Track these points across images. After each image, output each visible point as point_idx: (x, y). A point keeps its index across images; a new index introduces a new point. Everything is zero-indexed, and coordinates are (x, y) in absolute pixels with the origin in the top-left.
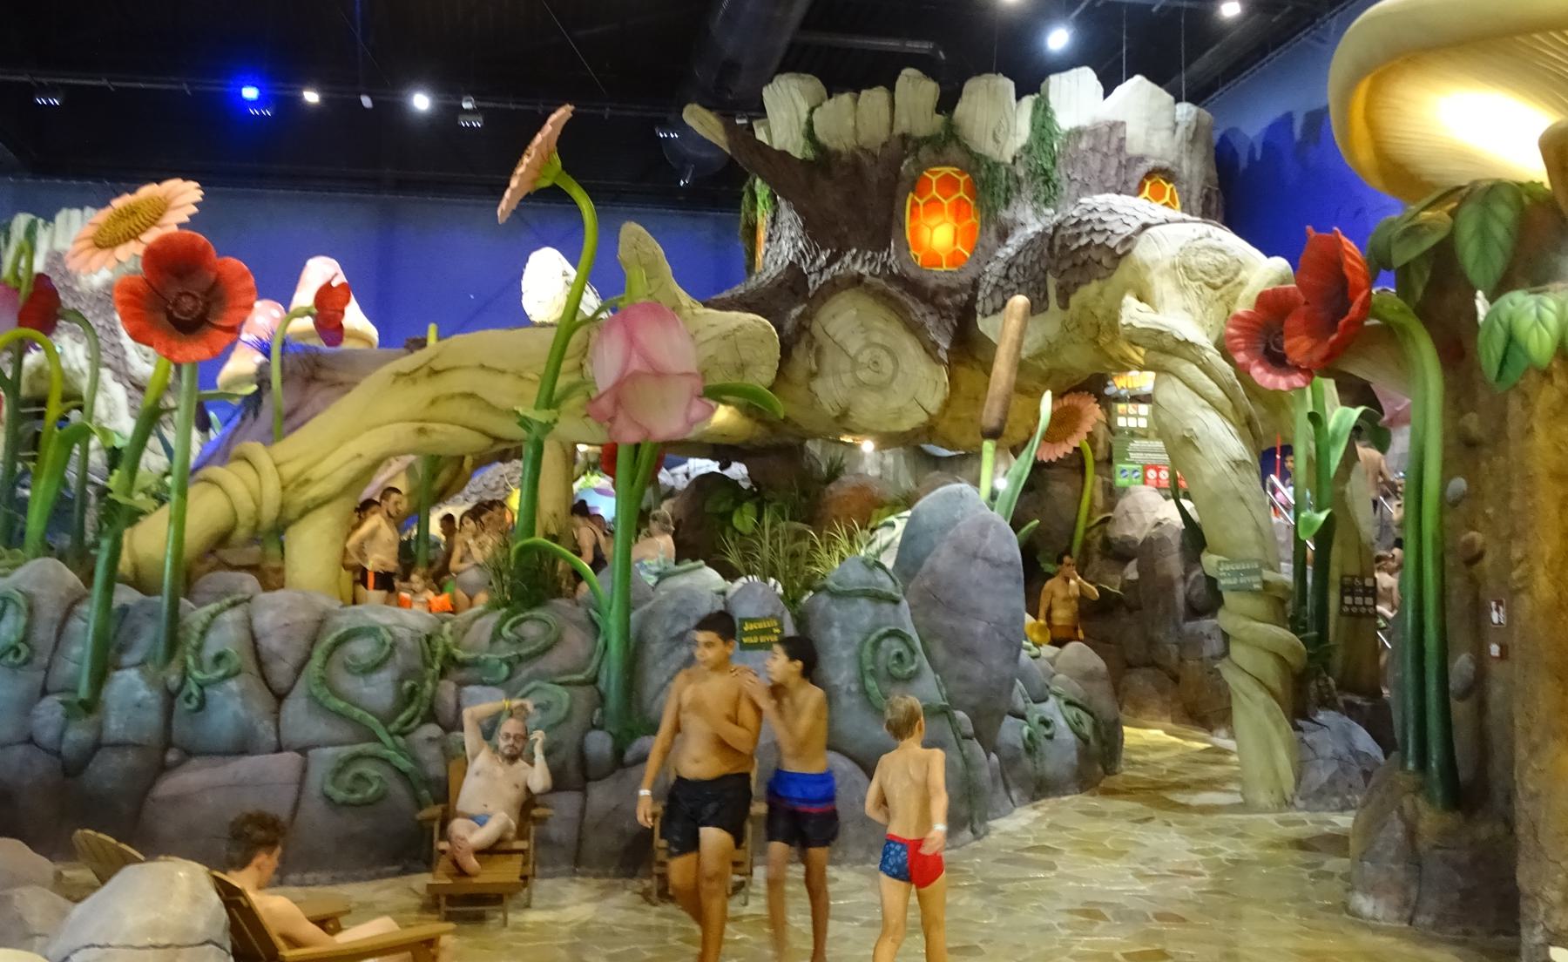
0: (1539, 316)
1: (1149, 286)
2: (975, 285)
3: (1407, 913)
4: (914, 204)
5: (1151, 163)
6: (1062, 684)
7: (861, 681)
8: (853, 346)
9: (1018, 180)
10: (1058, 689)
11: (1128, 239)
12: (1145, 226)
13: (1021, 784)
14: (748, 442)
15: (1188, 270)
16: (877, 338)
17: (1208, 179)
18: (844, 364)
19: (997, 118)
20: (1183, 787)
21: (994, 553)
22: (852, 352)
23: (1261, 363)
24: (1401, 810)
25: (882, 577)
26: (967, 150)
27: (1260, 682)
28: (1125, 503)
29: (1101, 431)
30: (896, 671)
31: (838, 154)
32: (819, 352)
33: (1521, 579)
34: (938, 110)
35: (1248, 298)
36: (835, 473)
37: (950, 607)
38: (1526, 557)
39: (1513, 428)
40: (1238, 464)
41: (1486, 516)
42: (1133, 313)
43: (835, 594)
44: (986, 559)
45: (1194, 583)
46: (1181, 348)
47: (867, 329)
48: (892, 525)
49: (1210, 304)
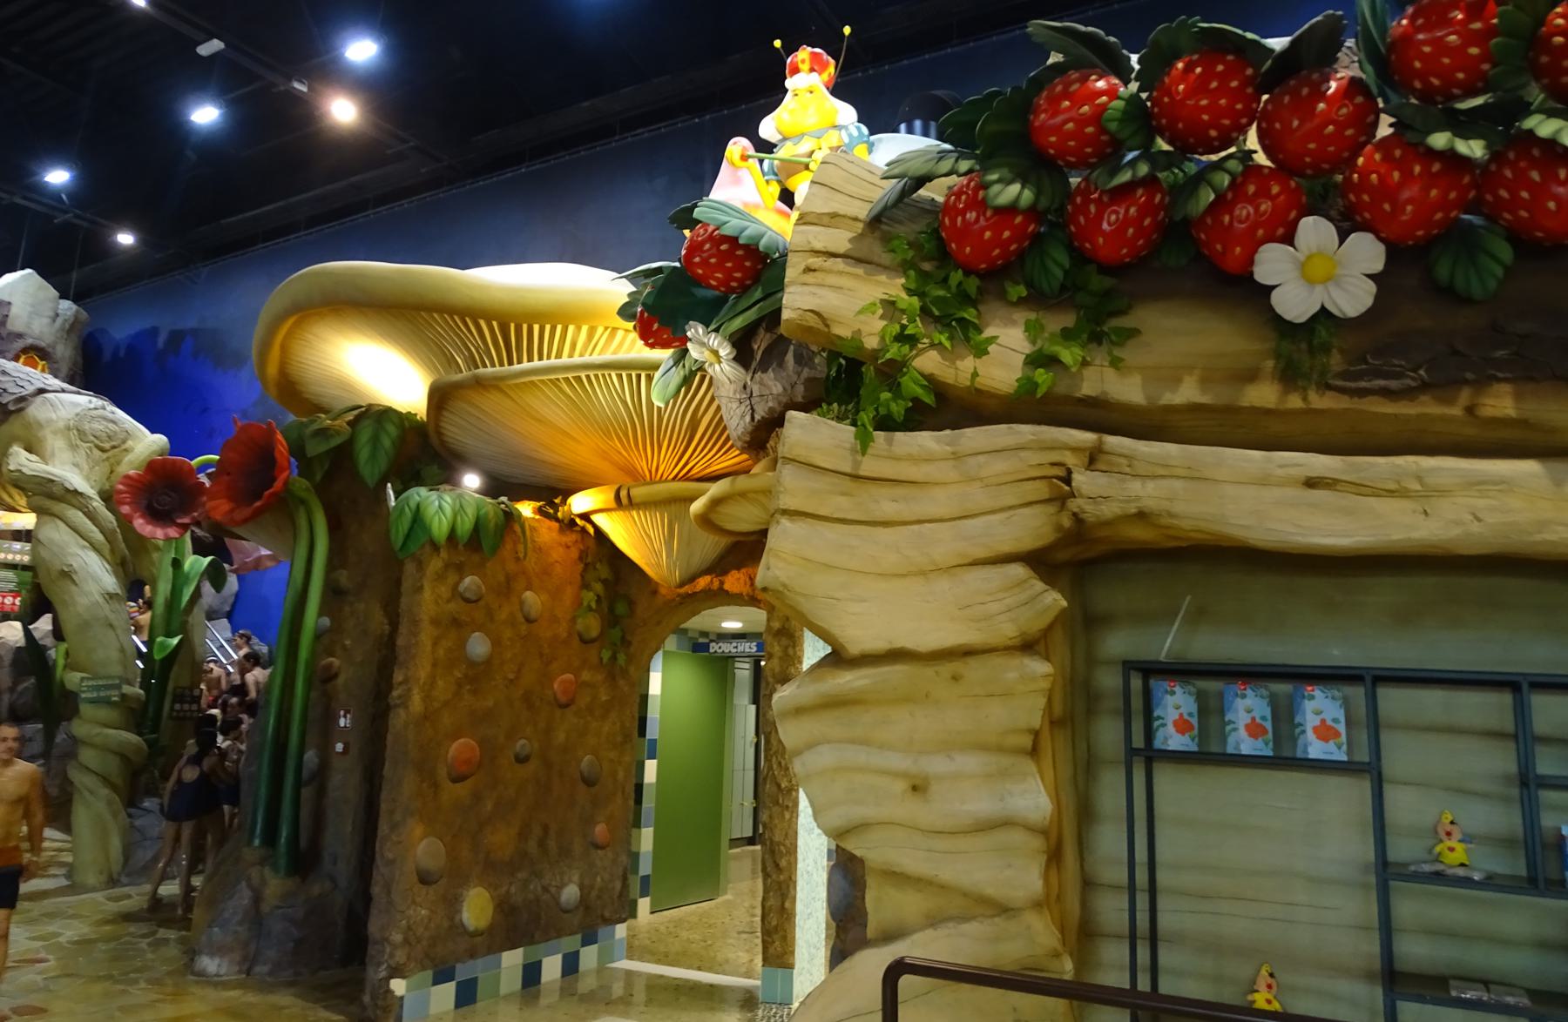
0: (440, 507)
1: (40, 441)
3: (245, 968)
5: (30, 341)
11: (22, 399)
12: (42, 391)
15: (81, 433)
17: (75, 364)
23: (142, 516)
24: (249, 880)
33: (400, 697)
35: (131, 462)
38: (406, 681)
39: (407, 585)
40: (111, 596)
41: (344, 648)
42: (21, 460)
45: (21, 693)
46: (69, 496)
49: (97, 463)
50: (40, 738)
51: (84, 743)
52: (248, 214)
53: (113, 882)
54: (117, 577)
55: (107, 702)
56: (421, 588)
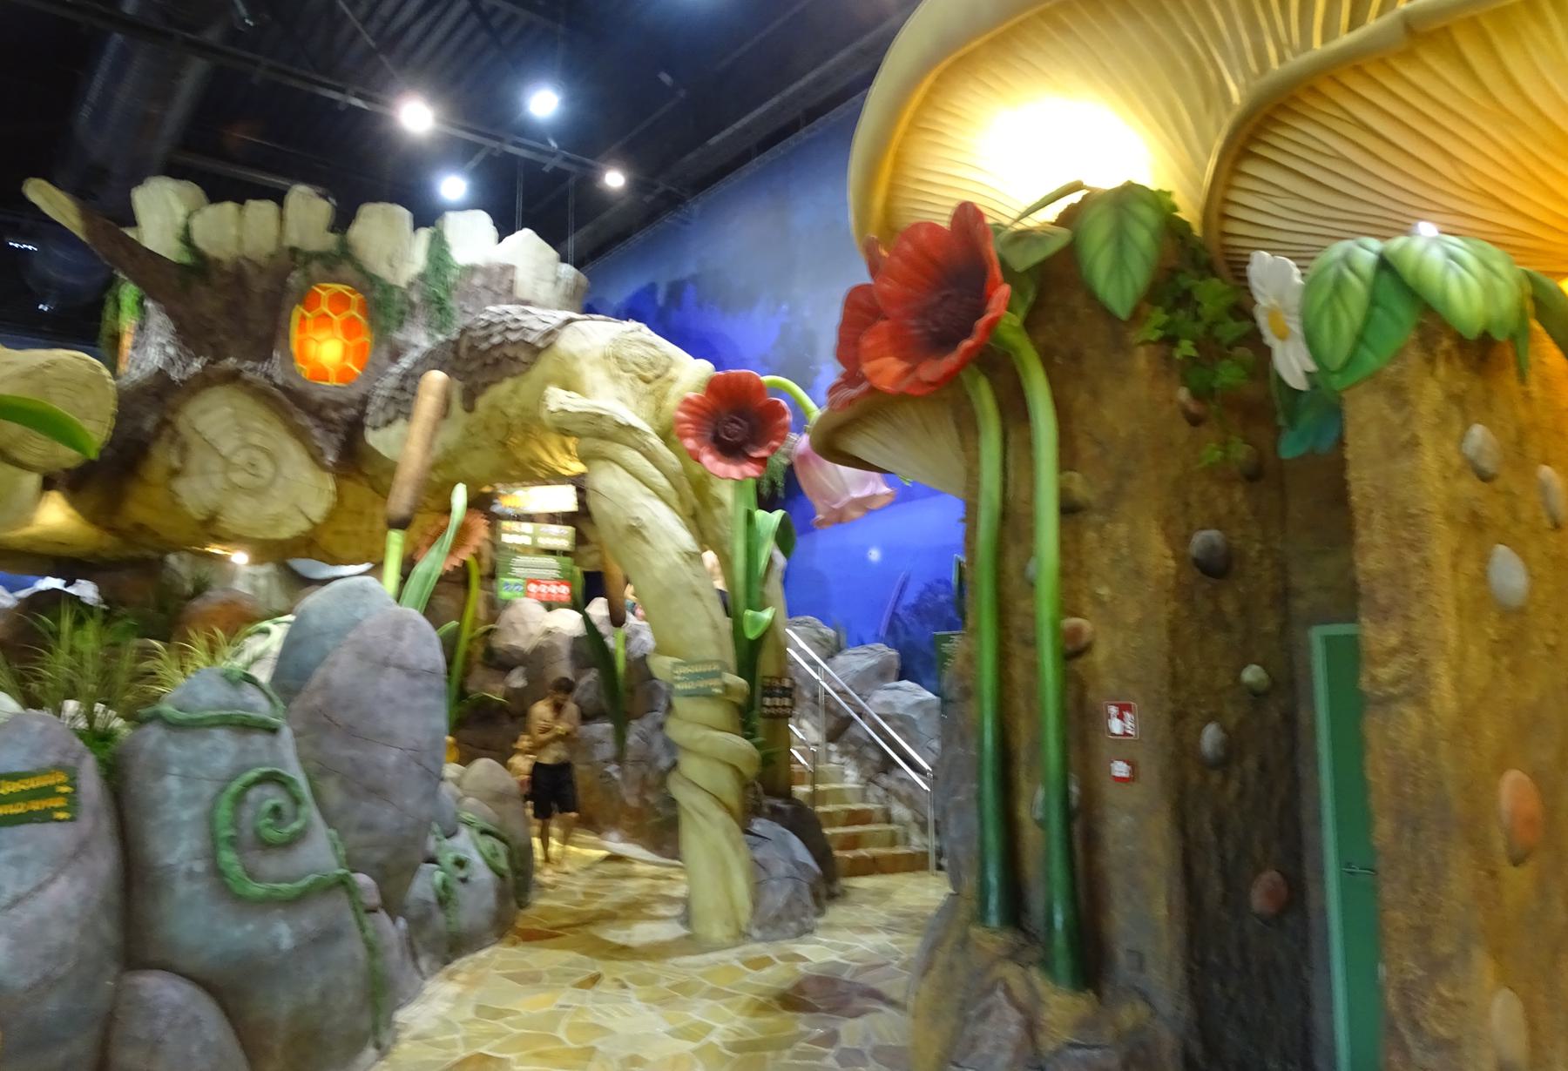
1: (577, 375)
2: (365, 401)
4: (303, 318)
6: (472, 810)
7: (212, 855)
8: (227, 445)
9: (412, 305)
10: (467, 816)
11: (550, 333)
13: (431, 948)
14: (94, 555)
16: (256, 439)
18: (214, 464)
19: (389, 242)
20: (608, 917)
21: (412, 660)
22: (225, 451)
23: (711, 452)
25: (253, 696)
26: (360, 268)
27: (718, 800)
28: (509, 614)
29: (486, 548)
30: (272, 834)
31: (218, 261)
32: (184, 449)
34: (332, 229)
36: (200, 588)
37: (351, 734)
38: (1409, 645)
41: (1097, 601)
42: (558, 399)
43: (173, 725)
44: (401, 667)
46: (622, 434)
47: (243, 429)
48: (267, 632)
50: (610, 739)
51: (687, 750)
52: (738, 125)
53: (742, 936)
54: (691, 532)
55: (707, 695)
56: (1413, 444)
